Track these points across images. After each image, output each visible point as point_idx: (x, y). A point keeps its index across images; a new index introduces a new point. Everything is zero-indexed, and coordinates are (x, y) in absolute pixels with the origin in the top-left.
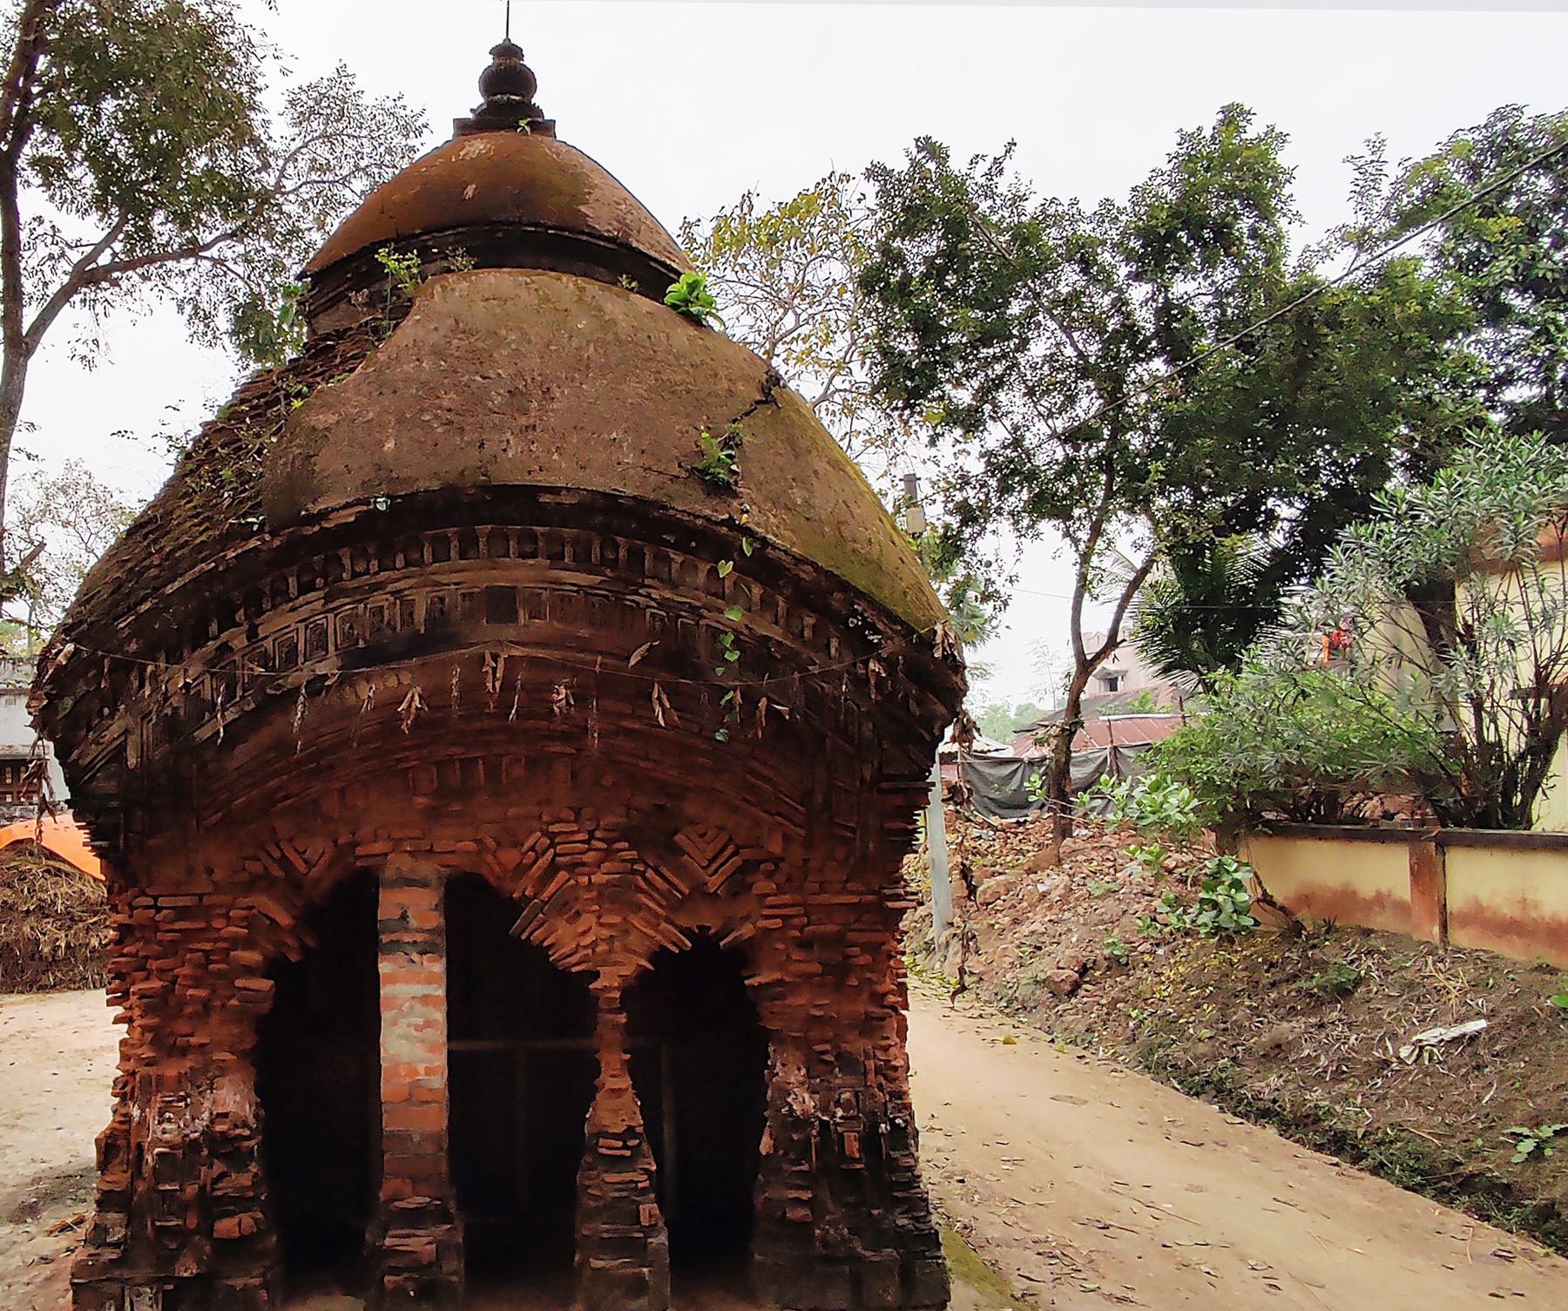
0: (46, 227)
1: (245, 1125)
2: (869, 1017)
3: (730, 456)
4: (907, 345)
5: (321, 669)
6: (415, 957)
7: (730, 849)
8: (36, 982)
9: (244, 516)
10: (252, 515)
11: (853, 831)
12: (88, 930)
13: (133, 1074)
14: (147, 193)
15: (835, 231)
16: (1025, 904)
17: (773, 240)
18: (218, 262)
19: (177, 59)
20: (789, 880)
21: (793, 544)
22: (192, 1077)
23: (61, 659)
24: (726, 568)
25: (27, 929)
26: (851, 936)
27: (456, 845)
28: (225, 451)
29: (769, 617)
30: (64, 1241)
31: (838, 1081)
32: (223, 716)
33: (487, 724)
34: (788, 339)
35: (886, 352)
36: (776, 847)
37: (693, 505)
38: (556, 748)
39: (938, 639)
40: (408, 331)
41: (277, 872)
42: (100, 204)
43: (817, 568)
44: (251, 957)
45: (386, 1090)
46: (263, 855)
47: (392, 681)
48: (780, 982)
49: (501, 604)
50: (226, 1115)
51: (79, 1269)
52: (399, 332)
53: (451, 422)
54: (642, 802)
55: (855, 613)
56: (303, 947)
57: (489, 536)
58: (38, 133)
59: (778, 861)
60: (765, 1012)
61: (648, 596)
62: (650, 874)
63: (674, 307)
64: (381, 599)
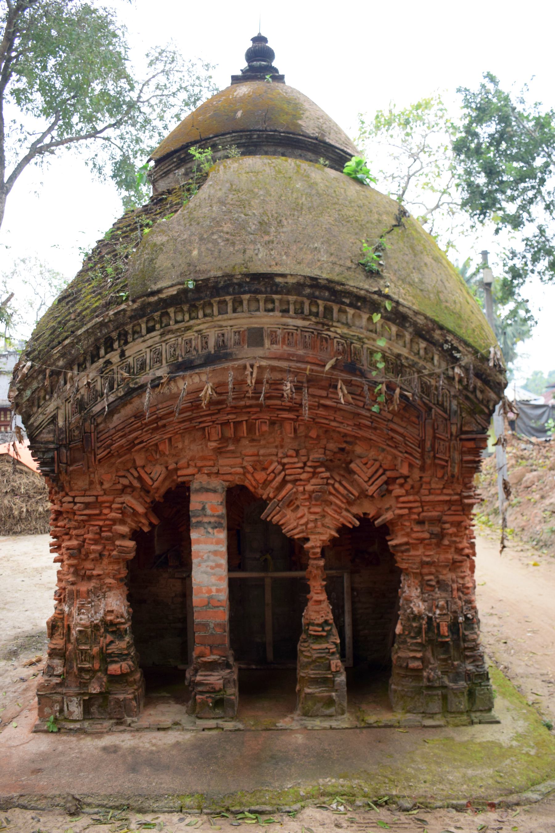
0: (18, 125)
1: (122, 616)
2: (454, 562)
3: (379, 256)
4: (481, 180)
5: (159, 373)
6: (210, 530)
7: (381, 471)
8: (11, 530)
9: (118, 292)
10: (123, 291)
11: (447, 461)
12: (37, 502)
13: (64, 589)
14: (70, 105)
15: (441, 117)
16: (547, 488)
17: (407, 122)
18: (108, 139)
19: (87, 39)
20: (412, 487)
21: (413, 304)
22: (94, 592)
23: (25, 370)
24: (377, 318)
25: (6, 502)
26: (445, 518)
27: (232, 468)
28: (109, 256)
29: (401, 343)
30: (32, 670)
31: (438, 595)
32: (107, 400)
33: (249, 402)
34: (417, 174)
35: (470, 184)
36: (405, 470)
37: (359, 283)
38: (286, 415)
39: (492, 356)
40: (206, 190)
41: (136, 484)
42: (45, 112)
43: (426, 318)
44: (123, 529)
45: (197, 599)
46: (128, 475)
47: (196, 379)
48: (407, 543)
49: (255, 337)
50: (112, 611)
51: (41, 687)
52: (201, 191)
53: (228, 240)
54: (332, 446)
55: (446, 342)
56: (151, 524)
57: (249, 301)
58: (14, 76)
59: (406, 478)
60: (398, 559)
61: (336, 332)
62: (337, 485)
63: (349, 174)
64: (189, 335)
